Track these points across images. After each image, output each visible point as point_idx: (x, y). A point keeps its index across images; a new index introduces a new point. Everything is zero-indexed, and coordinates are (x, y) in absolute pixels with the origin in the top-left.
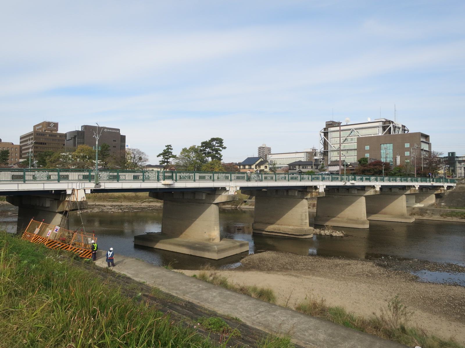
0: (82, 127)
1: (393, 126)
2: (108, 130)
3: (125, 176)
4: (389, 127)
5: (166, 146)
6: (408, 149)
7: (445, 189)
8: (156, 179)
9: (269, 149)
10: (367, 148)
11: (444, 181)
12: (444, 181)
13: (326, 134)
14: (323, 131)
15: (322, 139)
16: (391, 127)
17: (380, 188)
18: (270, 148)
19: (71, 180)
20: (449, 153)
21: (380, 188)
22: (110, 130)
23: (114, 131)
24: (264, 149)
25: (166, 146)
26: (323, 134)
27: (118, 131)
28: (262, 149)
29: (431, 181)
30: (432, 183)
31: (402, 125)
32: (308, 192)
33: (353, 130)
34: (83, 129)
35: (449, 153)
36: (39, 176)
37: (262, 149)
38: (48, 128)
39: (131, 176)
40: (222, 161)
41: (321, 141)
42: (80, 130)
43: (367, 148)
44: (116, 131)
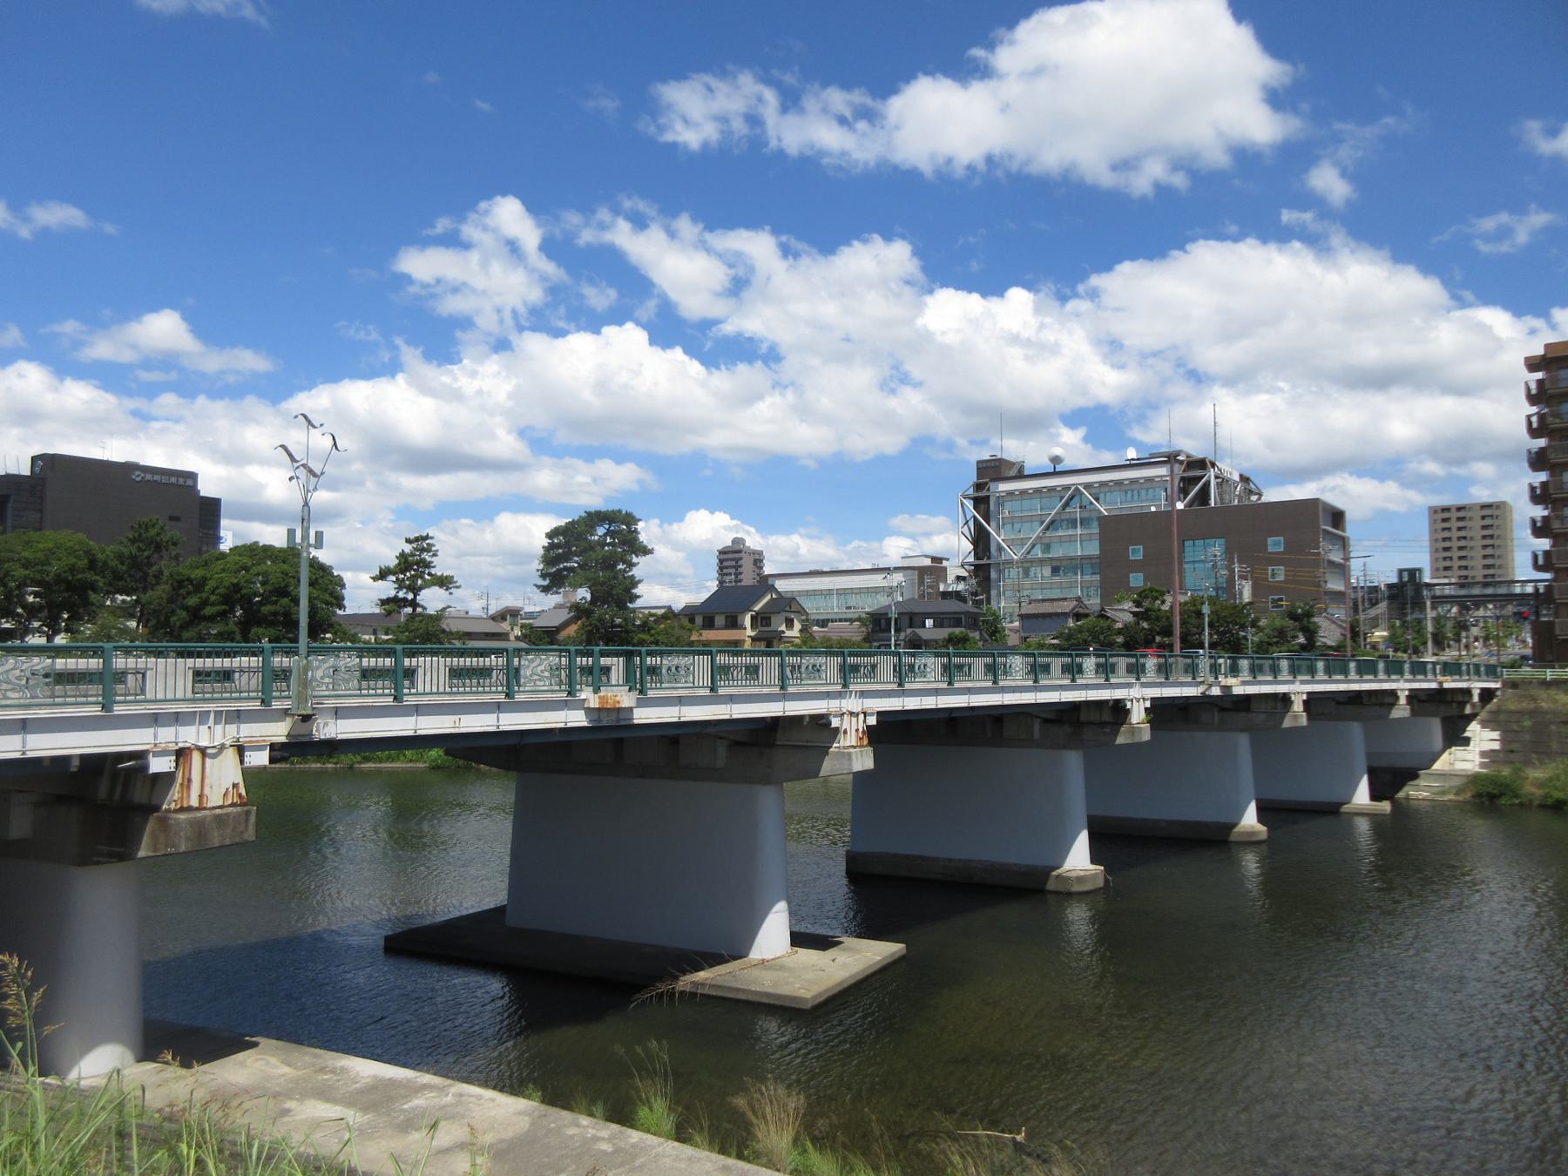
0: (34, 459)
1: (1216, 477)
2: (149, 477)
3: (140, 676)
4: (1203, 480)
5: (408, 541)
6: (1276, 560)
7: (1476, 699)
8: (621, 682)
9: (757, 557)
10: (1137, 553)
11: (1472, 672)
12: (1472, 672)
13: (981, 503)
14: (971, 491)
15: (967, 522)
16: (1207, 484)
17: (1146, 709)
18: (760, 553)
19: (176, 700)
20: (1401, 572)
21: (1146, 709)
22: (157, 478)
23: (173, 480)
24: (737, 556)
25: (408, 541)
26: (969, 504)
27: (190, 482)
28: (730, 556)
29: (1438, 672)
30: (1231, 681)
31: (1241, 476)
32: (1083, 723)
33: (1077, 489)
34: (37, 469)
35: (1401, 572)
36: (322, 678)
37: (730, 556)
38: (1452, 577)
39: (428, 674)
40: (639, 603)
41: (965, 530)
42: (26, 471)
43: (1137, 553)
44: (181, 481)
